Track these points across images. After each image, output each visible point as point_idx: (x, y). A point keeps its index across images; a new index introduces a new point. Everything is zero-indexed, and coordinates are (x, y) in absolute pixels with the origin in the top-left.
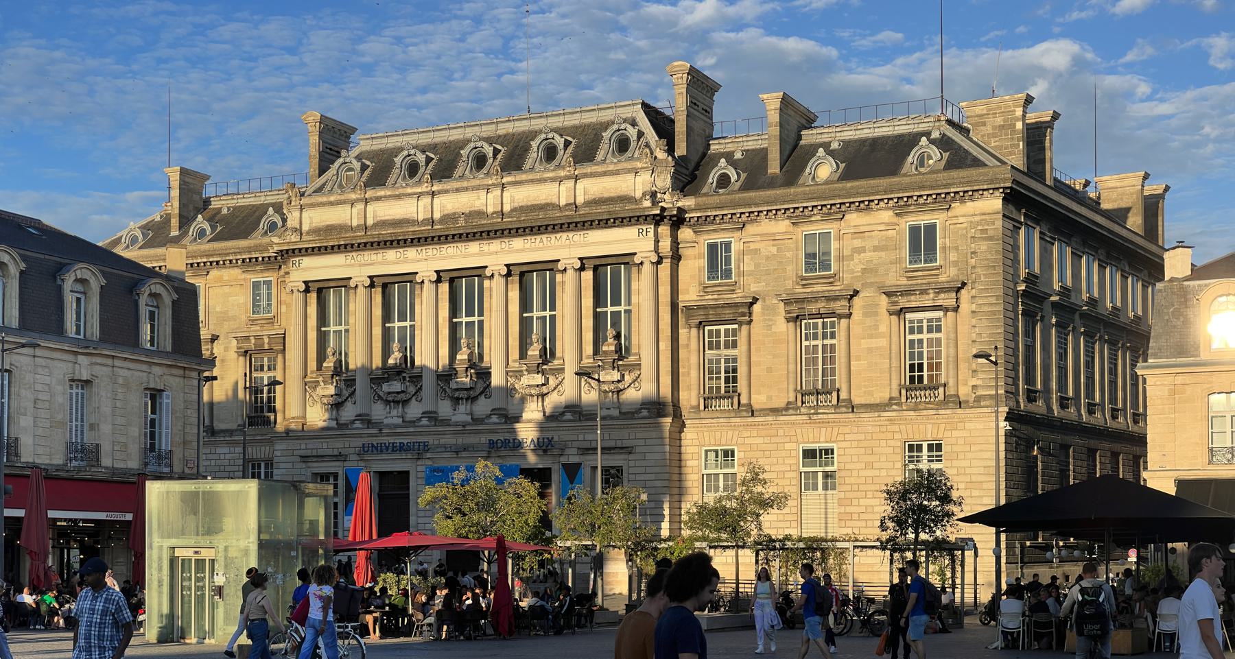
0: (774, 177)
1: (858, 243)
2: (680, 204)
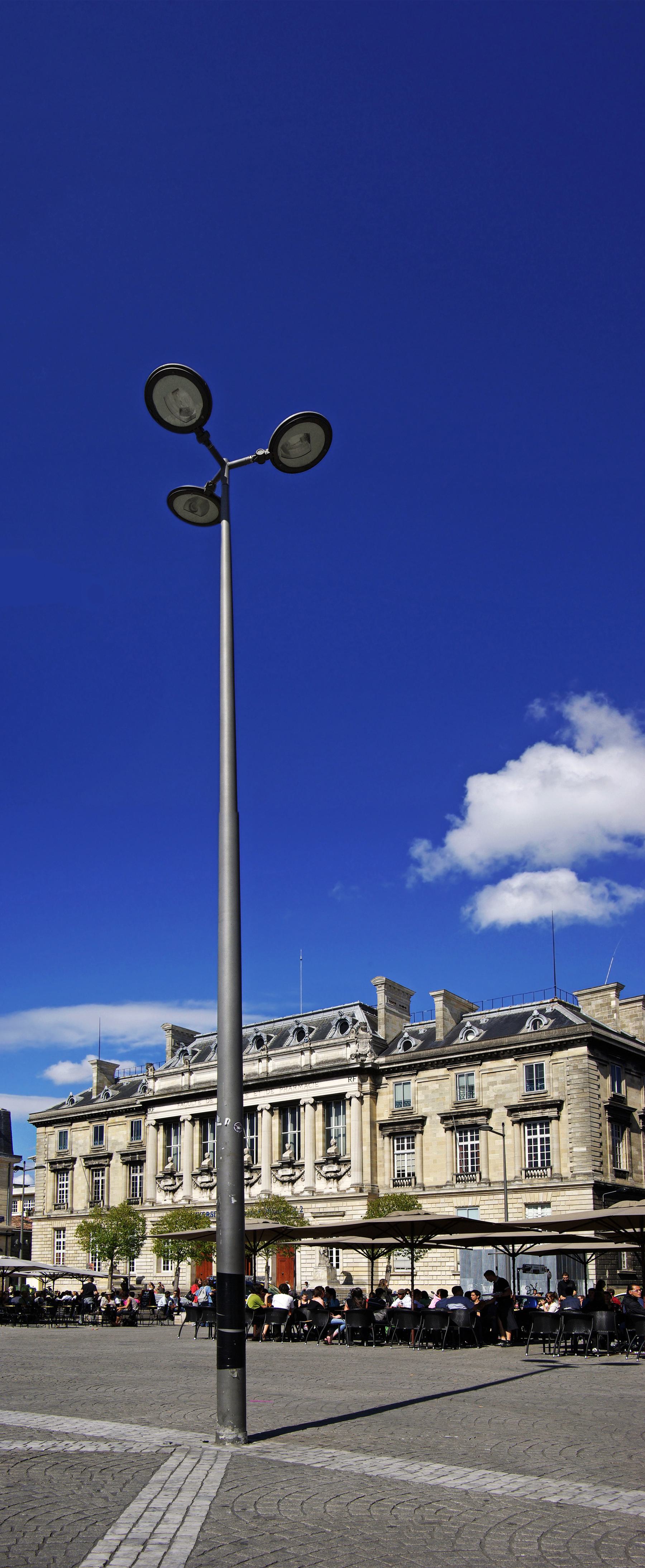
0: (439, 1042)
1: (491, 1078)
2: (376, 1062)
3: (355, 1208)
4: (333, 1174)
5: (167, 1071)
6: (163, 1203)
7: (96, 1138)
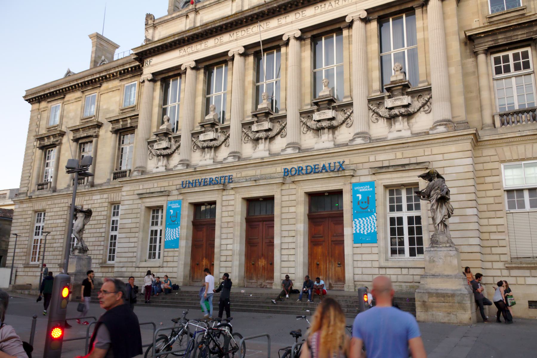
3: (446, 156)
4: (403, 110)
6: (155, 170)
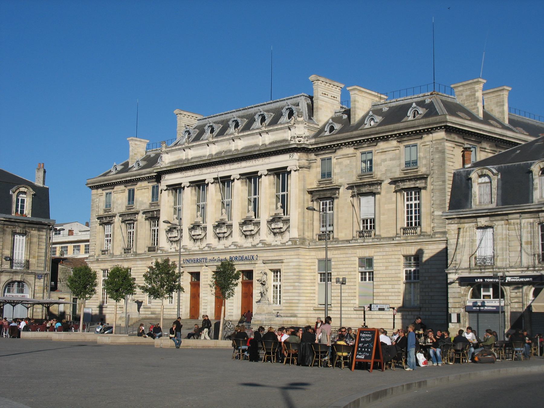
1: (383, 157)
4: (278, 230)
5: (174, 148)
6: (170, 251)
7: (129, 200)
